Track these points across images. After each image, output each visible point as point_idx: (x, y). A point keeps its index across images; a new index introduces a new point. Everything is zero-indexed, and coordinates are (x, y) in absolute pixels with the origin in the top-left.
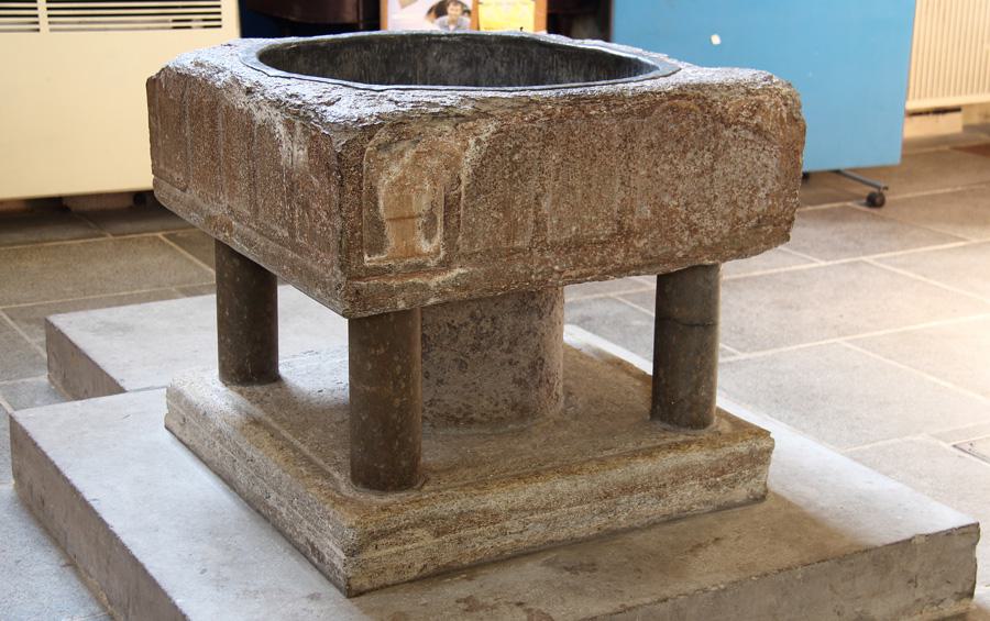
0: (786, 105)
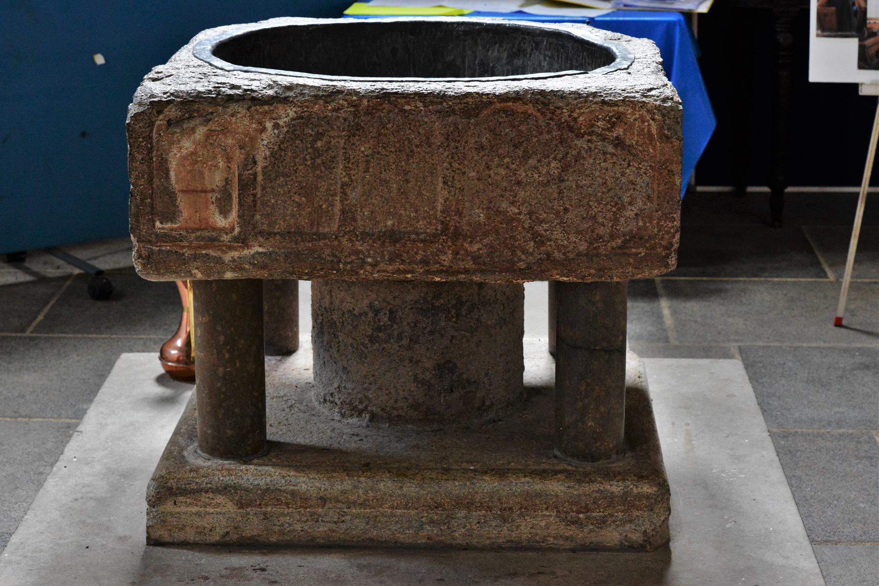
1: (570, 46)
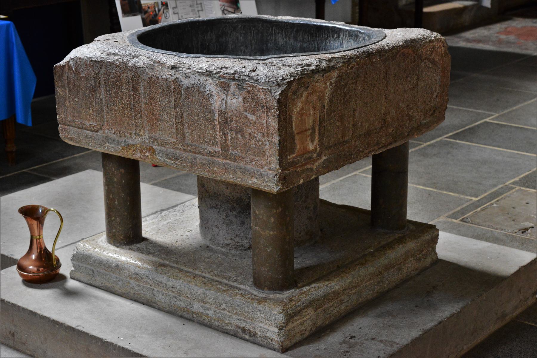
0: (444, 46)
1: (260, 25)
